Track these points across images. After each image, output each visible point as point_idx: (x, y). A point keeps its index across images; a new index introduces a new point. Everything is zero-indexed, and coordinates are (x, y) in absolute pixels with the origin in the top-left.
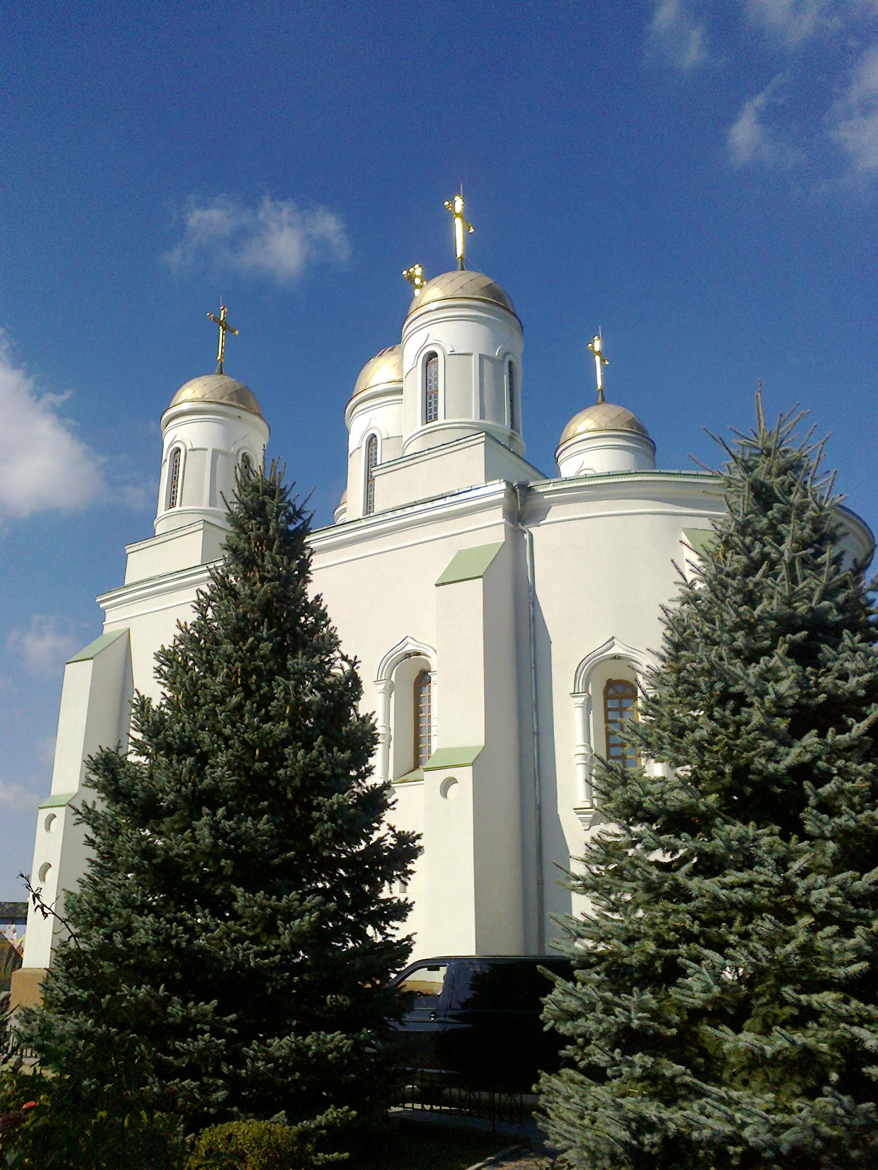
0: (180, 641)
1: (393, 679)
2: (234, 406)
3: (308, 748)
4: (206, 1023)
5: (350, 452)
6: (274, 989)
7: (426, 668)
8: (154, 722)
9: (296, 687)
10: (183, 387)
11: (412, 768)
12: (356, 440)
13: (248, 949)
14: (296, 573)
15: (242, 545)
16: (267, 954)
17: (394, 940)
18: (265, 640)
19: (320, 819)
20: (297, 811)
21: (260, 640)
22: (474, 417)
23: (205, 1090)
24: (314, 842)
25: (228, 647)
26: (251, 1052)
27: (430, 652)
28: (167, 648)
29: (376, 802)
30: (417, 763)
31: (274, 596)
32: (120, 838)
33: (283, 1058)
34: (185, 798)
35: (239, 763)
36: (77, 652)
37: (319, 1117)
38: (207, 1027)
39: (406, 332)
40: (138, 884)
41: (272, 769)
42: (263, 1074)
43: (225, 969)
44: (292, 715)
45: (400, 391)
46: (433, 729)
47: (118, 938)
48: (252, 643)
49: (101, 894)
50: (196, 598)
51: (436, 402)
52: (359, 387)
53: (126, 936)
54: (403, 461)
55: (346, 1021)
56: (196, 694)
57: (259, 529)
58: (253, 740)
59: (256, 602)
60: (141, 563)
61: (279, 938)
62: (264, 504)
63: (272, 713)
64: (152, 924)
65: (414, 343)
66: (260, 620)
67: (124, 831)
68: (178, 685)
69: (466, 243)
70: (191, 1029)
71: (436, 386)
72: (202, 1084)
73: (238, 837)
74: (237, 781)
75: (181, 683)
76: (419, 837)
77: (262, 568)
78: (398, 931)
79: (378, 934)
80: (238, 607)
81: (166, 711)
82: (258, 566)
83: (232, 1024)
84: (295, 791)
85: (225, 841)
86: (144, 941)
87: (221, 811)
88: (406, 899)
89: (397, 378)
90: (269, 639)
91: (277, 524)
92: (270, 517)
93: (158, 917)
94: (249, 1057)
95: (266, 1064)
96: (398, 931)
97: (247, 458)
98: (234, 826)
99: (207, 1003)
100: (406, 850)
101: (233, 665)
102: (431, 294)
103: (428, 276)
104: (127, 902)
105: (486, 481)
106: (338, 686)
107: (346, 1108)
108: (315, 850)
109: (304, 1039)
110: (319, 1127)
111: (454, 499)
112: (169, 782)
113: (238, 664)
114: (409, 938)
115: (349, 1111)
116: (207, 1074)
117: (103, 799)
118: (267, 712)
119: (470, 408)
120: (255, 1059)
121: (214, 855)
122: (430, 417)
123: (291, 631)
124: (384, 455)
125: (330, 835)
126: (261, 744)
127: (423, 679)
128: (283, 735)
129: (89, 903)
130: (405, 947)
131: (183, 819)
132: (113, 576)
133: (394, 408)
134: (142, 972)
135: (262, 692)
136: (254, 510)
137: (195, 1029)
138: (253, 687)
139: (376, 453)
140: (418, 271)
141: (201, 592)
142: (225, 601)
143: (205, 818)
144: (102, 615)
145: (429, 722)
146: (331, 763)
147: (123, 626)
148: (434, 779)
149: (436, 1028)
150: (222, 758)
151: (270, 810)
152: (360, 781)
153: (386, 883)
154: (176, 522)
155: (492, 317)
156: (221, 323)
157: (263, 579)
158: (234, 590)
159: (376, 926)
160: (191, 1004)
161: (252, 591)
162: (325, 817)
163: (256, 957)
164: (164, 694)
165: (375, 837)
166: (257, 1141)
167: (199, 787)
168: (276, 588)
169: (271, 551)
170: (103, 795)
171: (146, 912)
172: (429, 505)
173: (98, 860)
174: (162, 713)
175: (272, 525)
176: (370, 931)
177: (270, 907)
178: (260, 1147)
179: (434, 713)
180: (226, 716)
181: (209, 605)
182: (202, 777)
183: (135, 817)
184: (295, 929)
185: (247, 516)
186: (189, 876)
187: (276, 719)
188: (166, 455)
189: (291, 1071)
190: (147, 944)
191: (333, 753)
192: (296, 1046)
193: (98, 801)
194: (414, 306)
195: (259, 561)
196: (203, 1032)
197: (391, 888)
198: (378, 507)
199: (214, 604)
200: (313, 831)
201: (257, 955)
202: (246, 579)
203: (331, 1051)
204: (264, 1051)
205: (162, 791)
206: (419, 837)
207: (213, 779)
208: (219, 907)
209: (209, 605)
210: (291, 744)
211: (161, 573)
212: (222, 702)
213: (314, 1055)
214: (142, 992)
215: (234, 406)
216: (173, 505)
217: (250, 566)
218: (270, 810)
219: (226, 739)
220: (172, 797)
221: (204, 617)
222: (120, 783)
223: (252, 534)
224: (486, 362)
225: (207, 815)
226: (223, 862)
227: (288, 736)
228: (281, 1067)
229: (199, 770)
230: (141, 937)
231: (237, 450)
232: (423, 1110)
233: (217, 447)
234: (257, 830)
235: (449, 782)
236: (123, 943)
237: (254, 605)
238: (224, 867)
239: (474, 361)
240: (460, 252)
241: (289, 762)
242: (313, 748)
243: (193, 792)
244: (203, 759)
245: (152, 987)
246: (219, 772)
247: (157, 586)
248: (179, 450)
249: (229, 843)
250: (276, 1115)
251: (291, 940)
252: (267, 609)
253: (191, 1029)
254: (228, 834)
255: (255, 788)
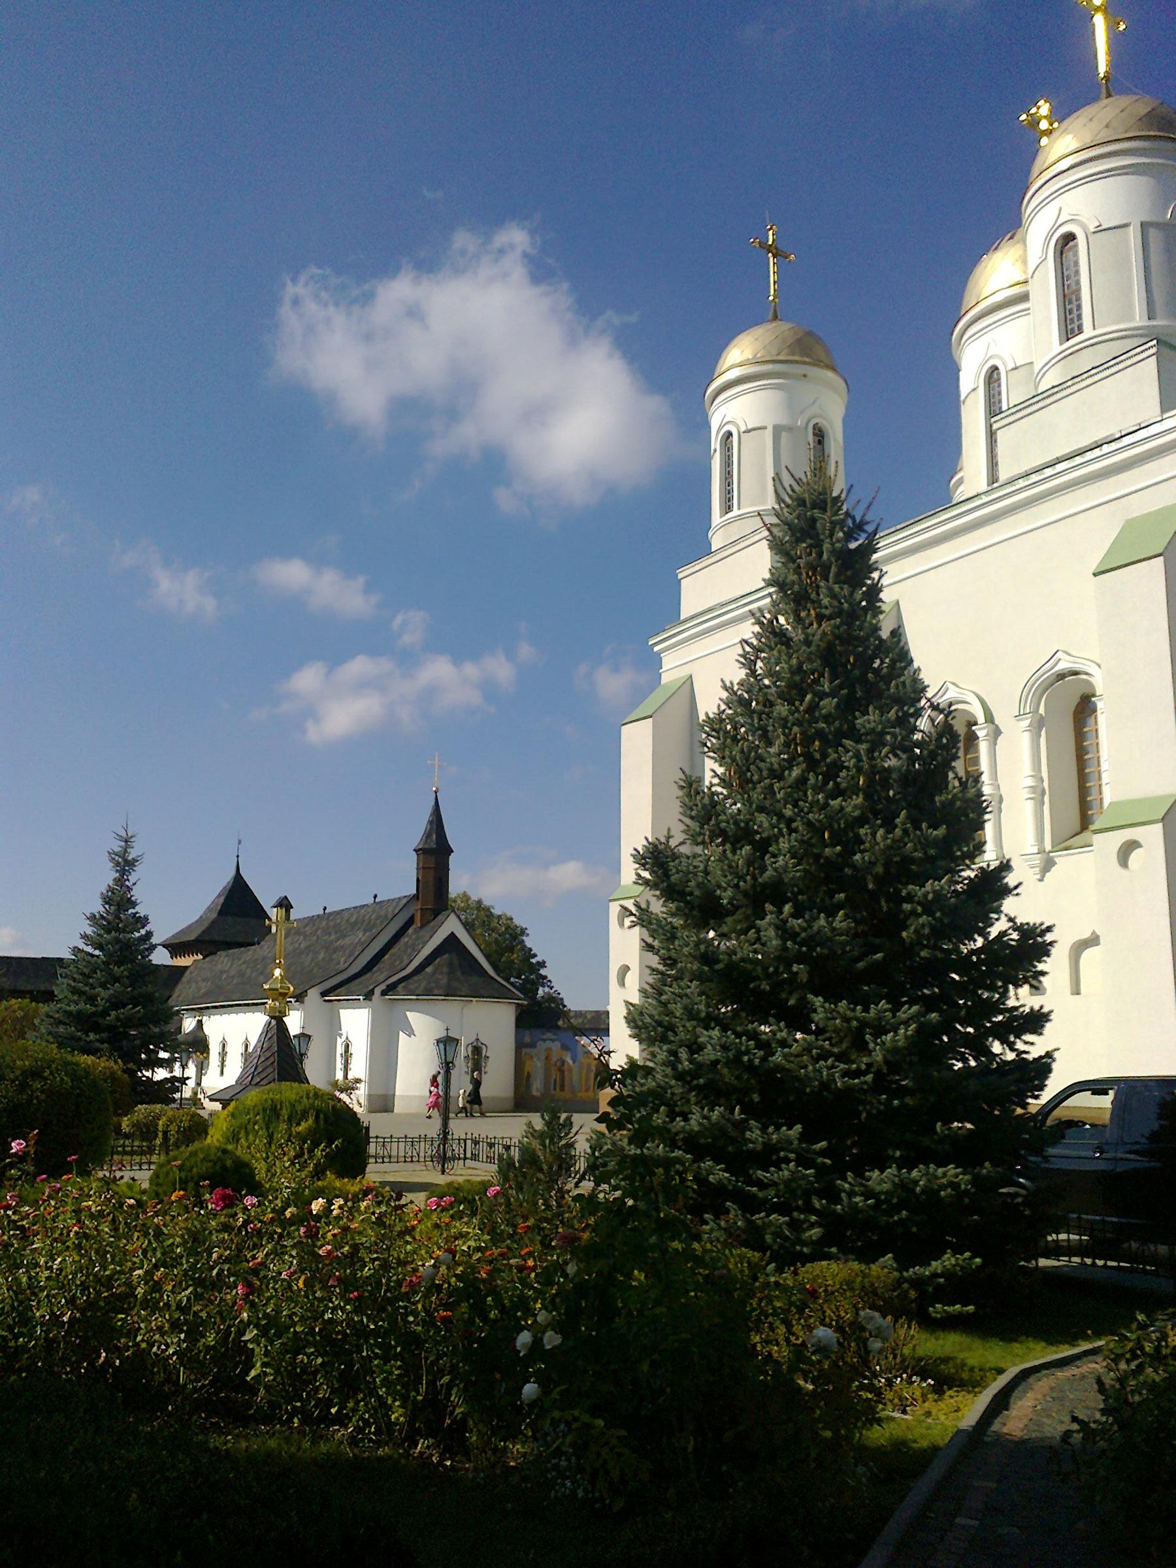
0: (727, 704)
1: (1042, 711)
2: (796, 362)
3: (889, 826)
4: (792, 1152)
5: (962, 398)
6: (869, 1113)
7: (1088, 691)
8: (704, 806)
9: (870, 751)
10: (729, 348)
11: (1078, 829)
12: (970, 379)
13: (833, 1067)
14: (864, 603)
15: (793, 577)
16: (858, 1073)
17: (1030, 1057)
18: (827, 695)
19: (913, 913)
20: (883, 903)
21: (822, 696)
22: (1139, 319)
23: (794, 1225)
24: (908, 940)
25: (782, 709)
26: (847, 1186)
27: (1092, 669)
28: (711, 716)
29: (993, 887)
30: (1085, 822)
31: (837, 637)
32: (677, 942)
33: (887, 1193)
34: (746, 894)
35: (806, 850)
36: (630, 713)
37: (934, 1263)
38: (792, 1156)
39: (1028, 209)
40: (700, 994)
41: (848, 852)
42: (861, 1211)
43: (808, 1090)
44: (868, 786)
45: (1024, 297)
46: (1104, 775)
47: (683, 1054)
48: (812, 701)
49: (665, 1004)
50: (741, 652)
51: (1079, 307)
52: (969, 299)
53: (692, 1052)
54: (1038, 400)
55: (962, 1152)
56: (749, 770)
57: (810, 554)
58: (820, 821)
59: (813, 648)
60: (698, 589)
61: (870, 1055)
62: (814, 520)
63: (844, 785)
64: (719, 1039)
65: (1041, 222)
66: (820, 669)
67: (679, 934)
68: (728, 760)
69: (1111, 51)
70: (774, 1157)
71: (1078, 283)
72: (792, 1219)
73: (812, 938)
74: (805, 870)
75: (731, 757)
76: (1049, 929)
77: (817, 603)
78: (1035, 1046)
79: (1008, 1051)
80: (790, 657)
81: (719, 789)
82: (813, 602)
83: (823, 1153)
84: (877, 879)
85: (795, 943)
86: (713, 1057)
87: (787, 908)
88: (1042, 1007)
89: (1022, 278)
90: (832, 694)
91: (833, 544)
92: (822, 537)
93: (724, 1029)
94: (845, 1191)
95: (866, 1200)
96: (1035, 1046)
97: (820, 430)
98: (805, 925)
99: (790, 1128)
100: (1030, 948)
101: (791, 730)
102: (1061, 146)
103: (1060, 114)
104: (691, 1014)
105: (1163, 411)
106: (928, 744)
107: (967, 1254)
108: (908, 950)
109: (909, 1172)
110: (935, 1275)
111: (1114, 446)
112: (726, 876)
113: (796, 729)
114: (1049, 1055)
115: (971, 1258)
116: (798, 1209)
117: (658, 898)
118: (837, 785)
119: (1130, 306)
120: (851, 1194)
121: (784, 959)
122: (1072, 329)
123: (863, 680)
124: (1011, 395)
125: (927, 931)
126: (831, 825)
127: (1085, 708)
128: (857, 813)
129: (651, 1016)
130: (1042, 1067)
131: (747, 918)
132: (664, 611)
133: (1022, 322)
134: (712, 1093)
135: (828, 760)
136: (802, 530)
137: (779, 1157)
138: (817, 756)
139: (1000, 394)
140: (1044, 108)
141: (746, 642)
142: (775, 652)
143: (769, 917)
144: (656, 662)
145: (1099, 765)
146: (920, 843)
147: (683, 672)
148: (1107, 844)
149: (1102, 1166)
150: (784, 844)
151: (849, 903)
152: (967, 862)
153: (1011, 987)
154: (736, 531)
155: (1160, 161)
156: (769, 249)
157: (820, 618)
158: (784, 635)
159: (1004, 1041)
160: (771, 1129)
161: (807, 635)
162: (919, 909)
163: (843, 1077)
164: (714, 771)
165: (994, 932)
166: (850, 1284)
167: (760, 880)
168: (838, 627)
169: (827, 581)
170: (658, 893)
171: (713, 1025)
172: (1078, 460)
173: (661, 967)
174: (713, 794)
175: (826, 546)
176: (997, 1047)
177: (857, 1019)
178: (852, 1289)
179: (1104, 753)
180: (786, 793)
181: (757, 658)
182: (763, 869)
183: (694, 917)
184: (888, 1045)
185: (793, 539)
186: (758, 983)
187: (849, 793)
188: (716, 444)
189: (897, 1209)
190: (717, 1062)
191: (920, 829)
192: (901, 1180)
193: (653, 900)
194: (1036, 170)
195: (813, 596)
196: (787, 1161)
197: (1016, 994)
198: (1004, 475)
199: (763, 655)
200: (906, 928)
201: (845, 1073)
202: (798, 620)
203: (943, 1187)
204: (862, 1185)
205: (719, 887)
206: (1049, 929)
207: (775, 870)
208: (798, 1019)
209: (757, 658)
210: (867, 823)
211: (723, 599)
212: (780, 778)
213: (923, 1191)
214: (715, 1115)
215: (796, 362)
216: (729, 509)
217: (803, 603)
218: (849, 903)
219: (790, 821)
220: (729, 893)
221: (753, 672)
222: (673, 879)
223: (802, 562)
224: (1153, 233)
225: (771, 913)
226: (795, 968)
227: (863, 813)
228: (883, 1204)
229: (756, 862)
230: (710, 1054)
231: (805, 422)
232: (1083, 1264)
233: (778, 422)
234: (834, 929)
235: (1129, 847)
236: (691, 1061)
237: (811, 653)
238: (797, 973)
239: (1133, 236)
240: (1102, 68)
241: (867, 845)
242: (896, 826)
243: (753, 886)
244: (763, 847)
245: (726, 1109)
246: (781, 860)
247: (715, 617)
248: (730, 434)
249: (801, 945)
250: (882, 1260)
251: (884, 1056)
252: (829, 656)
253: (774, 1157)
254: (798, 934)
255: (828, 879)
